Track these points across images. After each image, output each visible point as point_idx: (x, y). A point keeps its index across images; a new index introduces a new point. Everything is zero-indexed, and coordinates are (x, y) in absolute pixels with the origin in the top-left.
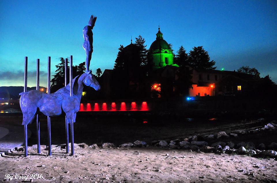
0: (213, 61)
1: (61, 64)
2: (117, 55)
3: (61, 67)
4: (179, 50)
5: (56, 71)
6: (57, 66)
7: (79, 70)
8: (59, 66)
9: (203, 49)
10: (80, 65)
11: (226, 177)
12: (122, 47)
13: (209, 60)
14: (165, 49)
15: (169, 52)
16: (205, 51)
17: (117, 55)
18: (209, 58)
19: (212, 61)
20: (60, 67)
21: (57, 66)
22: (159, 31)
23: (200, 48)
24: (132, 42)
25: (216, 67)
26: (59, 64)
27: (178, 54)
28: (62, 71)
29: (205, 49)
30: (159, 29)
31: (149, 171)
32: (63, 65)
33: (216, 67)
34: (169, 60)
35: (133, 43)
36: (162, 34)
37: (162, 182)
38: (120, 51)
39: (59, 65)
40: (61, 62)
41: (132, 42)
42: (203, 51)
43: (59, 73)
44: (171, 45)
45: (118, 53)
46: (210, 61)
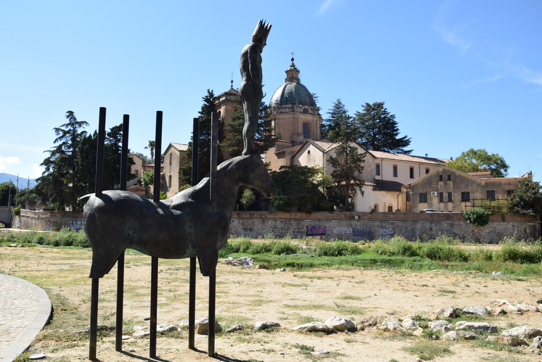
0: (406, 137)
1: (67, 125)
2: (199, 112)
3: (68, 132)
4: (332, 108)
5: (55, 142)
6: (57, 130)
7: (111, 140)
8: (62, 130)
9: (386, 109)
10: (111, 130)
11: (481, 314)
12: (211, 94)
13: (396, 134)
14: (304, 105)
15: (312, 112)
16: (390, 114)
17: (199, 112)
18: (398, 130)
19: (404, 138)
20: (65, 133)
21: (57, 130)
22: (293, 65)
23: (380, 105)
24: (232, 86)
25: (412, 150)
26: (64, 125)
27: (331, 118)
28: (70, 142)
29: (391, 109)
30: (293, 60)
31: (477, 195)
32: (72, 129)
33: (412, 150)
34: (312, 129)
35: (235, 88)
36: (299, 72)
37: (338, 358)
38: (206, 103)
39: (63, 128)
40: (67, 121)
41: (232, 86)
42: (385, 112)
43: (60, 146)
44: (315, 96)
45: (203, 108)
46: (398, 137)
